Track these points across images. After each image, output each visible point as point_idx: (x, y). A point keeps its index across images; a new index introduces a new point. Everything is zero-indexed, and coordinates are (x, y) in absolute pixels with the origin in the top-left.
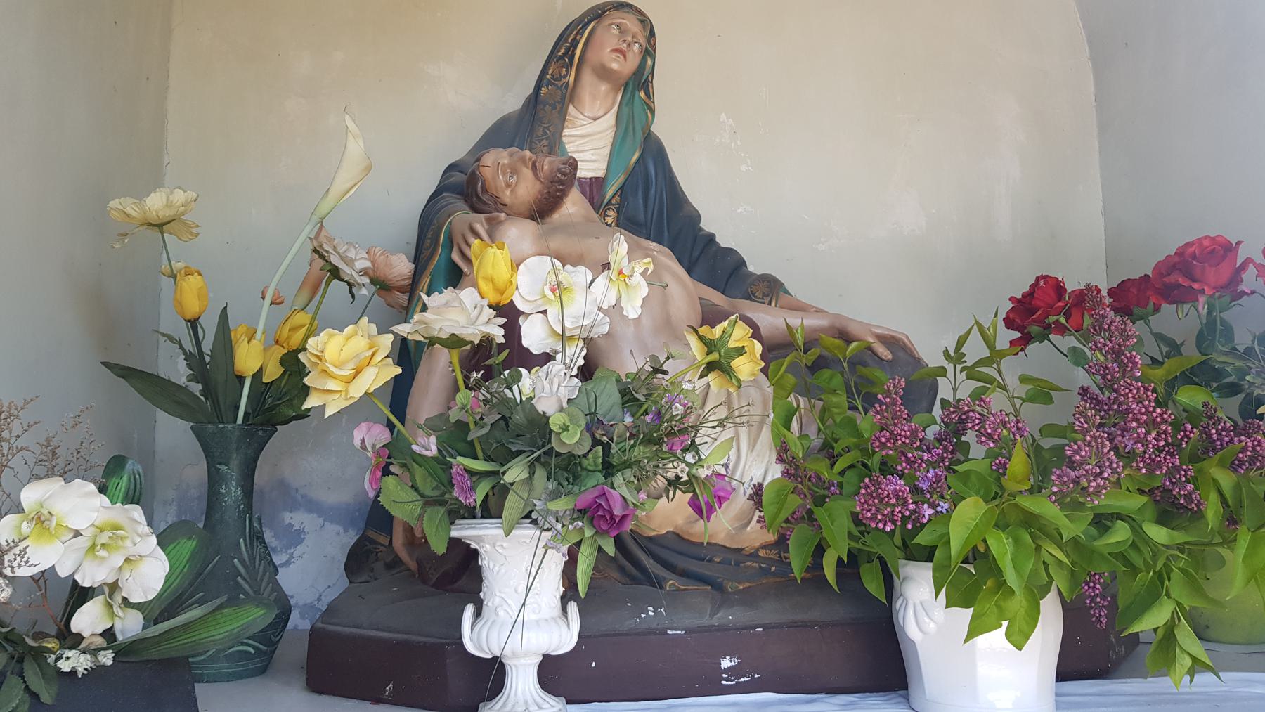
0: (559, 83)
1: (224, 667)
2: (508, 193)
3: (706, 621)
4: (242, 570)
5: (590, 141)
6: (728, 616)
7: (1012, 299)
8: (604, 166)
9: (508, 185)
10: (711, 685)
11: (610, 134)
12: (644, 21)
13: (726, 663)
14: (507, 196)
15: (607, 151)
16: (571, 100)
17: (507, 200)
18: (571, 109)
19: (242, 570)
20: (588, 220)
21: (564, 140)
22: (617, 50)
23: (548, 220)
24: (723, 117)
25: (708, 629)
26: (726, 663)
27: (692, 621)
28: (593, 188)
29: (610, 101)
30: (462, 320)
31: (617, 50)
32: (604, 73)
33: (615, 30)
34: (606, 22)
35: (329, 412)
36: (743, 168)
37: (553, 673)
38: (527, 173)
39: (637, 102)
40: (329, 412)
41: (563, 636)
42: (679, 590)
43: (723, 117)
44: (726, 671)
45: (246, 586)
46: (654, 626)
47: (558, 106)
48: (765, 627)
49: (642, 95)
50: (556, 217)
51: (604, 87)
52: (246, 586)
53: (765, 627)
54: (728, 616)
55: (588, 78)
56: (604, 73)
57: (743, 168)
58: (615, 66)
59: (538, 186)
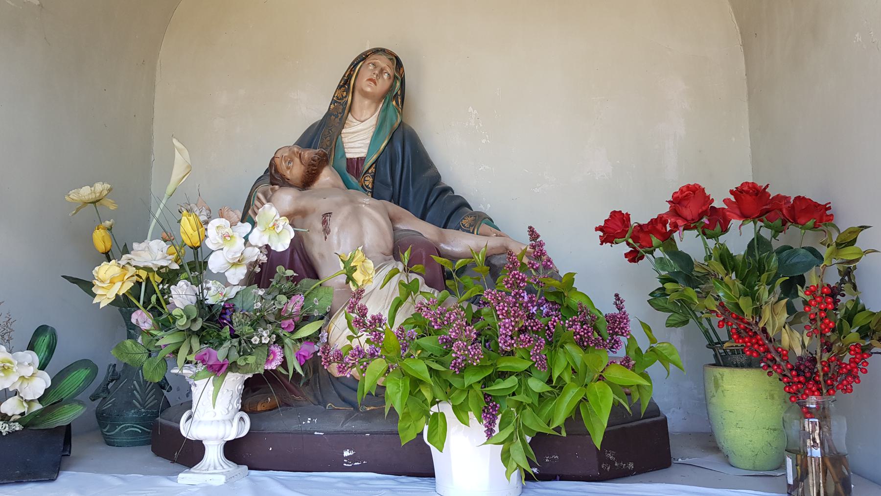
0: (342, 102)
1: (124, 439)
2: (288, 172)
3: (339, 428)
4: (138, 387)
5: (359, 138)
7: (597, 229)
8: (366, 151)
9: (288, 168)
10: (337, 466)
12: (363, 58)
13: (346, 453)
14: (288, 174)
15: (368, 141)
16: (350, 110)
17: (289, 177)
19: (138, 387)
21: (345, 140)
22: (370, 80)
23: (312, 187)
24: (470, 109)
25: (337, 433)
26: (346, 453)
27: (331, 427)
28: (354, 166)
29: (373, 109)
30: (149, 257)
31: (370, 80)
32: (365, 95)
33: (371, 67)
34: (367, 62)
35: (102, 306)
36: (484, 141)
37: (233, 451)
38: (297, 160)
39: (391, 108)
40: (102, 306)
41: (237, 428)
42: (334, 409)
43: (470, 109)
44: (347, 458)
45: (138, 396)
46: (308, 429)
47: (340, 116)
48: (371, 433)
49: (394, 103)
50: (316, 185)
51: (367, 102)
52: (138, 396)
53: (371, 433)
55: (357, 96)
56: (365, 95)
57: (484, 141)
58: (369, 89)
59: (303, 167)
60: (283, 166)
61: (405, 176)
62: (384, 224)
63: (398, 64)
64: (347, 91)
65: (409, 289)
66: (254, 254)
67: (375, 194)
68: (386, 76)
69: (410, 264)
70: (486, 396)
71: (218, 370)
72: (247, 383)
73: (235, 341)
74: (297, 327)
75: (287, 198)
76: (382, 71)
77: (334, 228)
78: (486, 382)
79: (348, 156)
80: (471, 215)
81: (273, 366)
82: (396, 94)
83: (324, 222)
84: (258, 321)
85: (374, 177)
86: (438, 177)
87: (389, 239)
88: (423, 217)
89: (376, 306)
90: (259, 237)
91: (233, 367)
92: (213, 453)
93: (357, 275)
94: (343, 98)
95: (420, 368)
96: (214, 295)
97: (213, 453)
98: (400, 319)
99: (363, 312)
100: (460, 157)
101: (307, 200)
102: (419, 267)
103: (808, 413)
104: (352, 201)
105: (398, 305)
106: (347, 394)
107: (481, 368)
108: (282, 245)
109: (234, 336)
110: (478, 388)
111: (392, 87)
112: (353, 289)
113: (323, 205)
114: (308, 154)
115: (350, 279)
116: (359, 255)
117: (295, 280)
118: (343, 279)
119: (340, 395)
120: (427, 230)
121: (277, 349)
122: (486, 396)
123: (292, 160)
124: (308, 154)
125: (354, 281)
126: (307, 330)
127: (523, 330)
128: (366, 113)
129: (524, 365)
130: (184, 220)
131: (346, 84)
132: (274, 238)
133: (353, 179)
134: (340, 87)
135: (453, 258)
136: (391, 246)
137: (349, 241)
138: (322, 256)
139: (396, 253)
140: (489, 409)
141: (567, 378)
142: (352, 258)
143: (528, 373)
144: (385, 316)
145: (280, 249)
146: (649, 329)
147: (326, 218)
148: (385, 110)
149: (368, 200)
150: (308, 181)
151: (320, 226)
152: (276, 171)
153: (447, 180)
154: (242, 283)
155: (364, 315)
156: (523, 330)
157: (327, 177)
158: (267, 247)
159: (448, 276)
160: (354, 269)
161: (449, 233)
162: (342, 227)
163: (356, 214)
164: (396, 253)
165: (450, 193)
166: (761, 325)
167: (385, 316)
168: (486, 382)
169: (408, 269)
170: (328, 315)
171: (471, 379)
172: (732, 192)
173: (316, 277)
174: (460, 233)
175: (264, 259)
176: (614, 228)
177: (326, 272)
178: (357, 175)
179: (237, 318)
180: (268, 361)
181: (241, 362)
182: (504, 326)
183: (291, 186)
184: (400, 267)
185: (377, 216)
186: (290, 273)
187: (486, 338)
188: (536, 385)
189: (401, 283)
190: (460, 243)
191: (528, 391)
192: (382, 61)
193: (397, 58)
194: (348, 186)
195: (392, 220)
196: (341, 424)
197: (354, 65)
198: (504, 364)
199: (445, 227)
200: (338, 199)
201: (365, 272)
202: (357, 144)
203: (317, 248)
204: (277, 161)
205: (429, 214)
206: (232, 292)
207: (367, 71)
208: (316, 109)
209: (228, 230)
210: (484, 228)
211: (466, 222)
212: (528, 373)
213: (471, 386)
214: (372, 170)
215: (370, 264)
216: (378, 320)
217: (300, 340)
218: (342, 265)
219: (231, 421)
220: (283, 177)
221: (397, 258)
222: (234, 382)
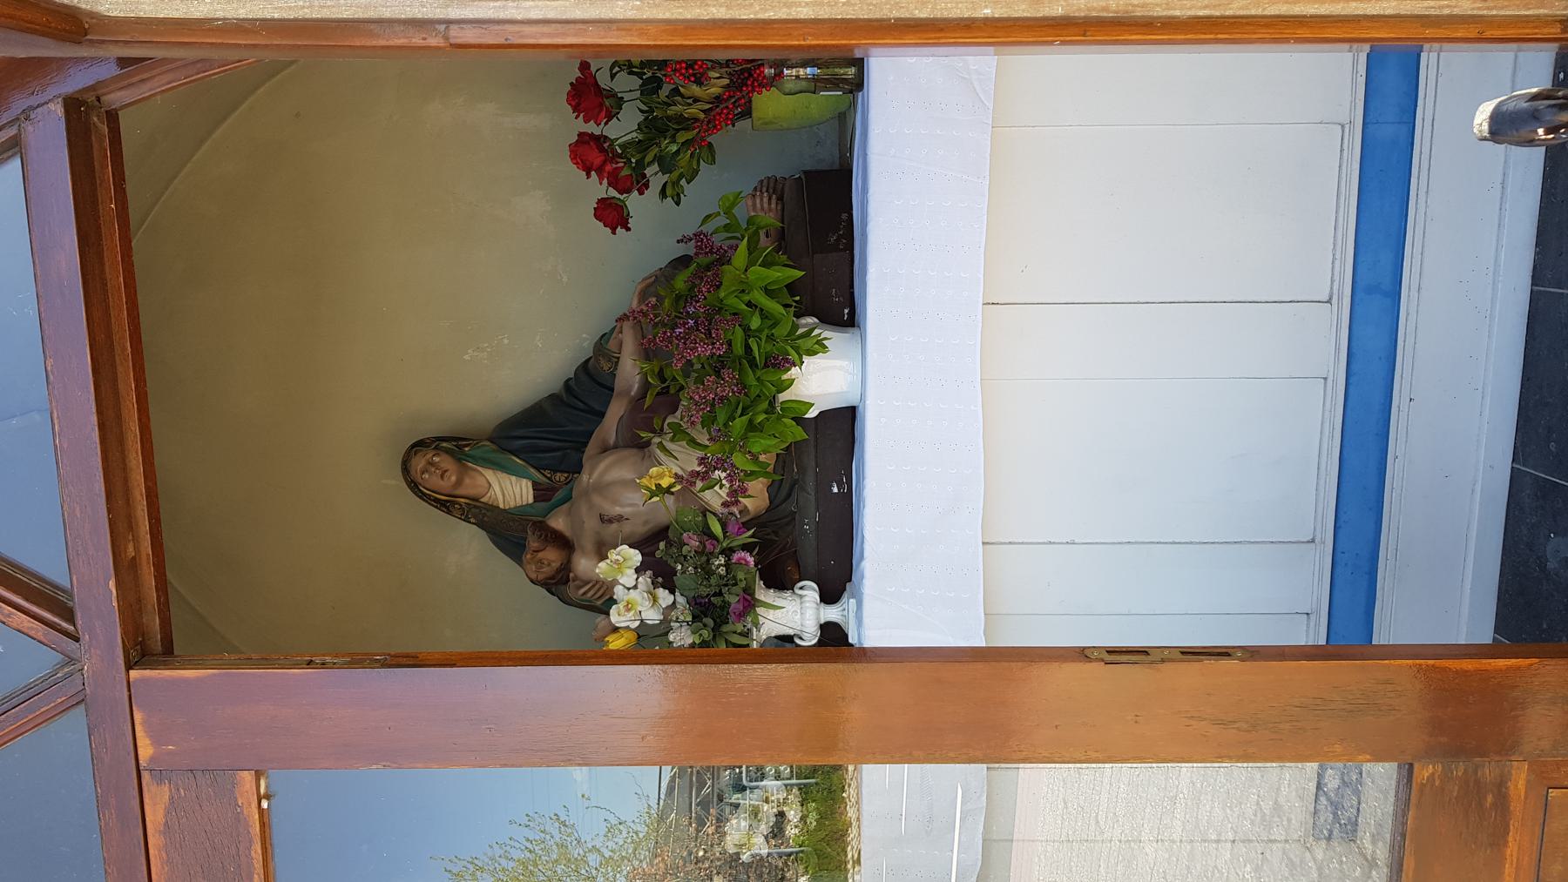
3: (812, 498)
5: (510, 489)
6: (810, 485)
8: (524, 481)
11: (501, 475)
12: (414, 486)
13: (835, 490)
14: (555, 565)
18: (484, 500)
20: (569, 513)
21: (512, 504)
24: (467, 357)
25: (817, 500)
28: (541, 493)
32: (459, 483)
33: (426, 476)
37: (830, 596)
38: (540, 555)
41: (810, 592)
43: (467, 357)
50: (568, 534)
51: (467, 481)
54: (810, 485)
56: (459, 483)
58: (453, 478)
60: (547, 570)
61: (554, 432)
62: (609, 459)
63: (420, 445)
64: (454, 503)
65: (678, 433)
66: (645, 580)
67: (577, 469)
68: (436, 459)
69: (653, 431)
70: (766, 366)
71: (750, 604)
72: (768, 586)
73: (725, 590)
74: (716, 538)
75: (583, 564)
76: (431, 464)
77: (618, 510)
78: (753, 364)
79: (531, 500)
80: (597, 361)
81: (751, 560)
82: (457, 445)
83: (610, 521)
84: (707, 572)
85: (555, 471)
86: (552, 397)
87: (626, 452)
88: (602, 415)
89: (689, 461)
90: (628, 577)
91: (749, 591)
92: (832, 613)
93: (665, 483)
94: (461, 508)
95: (739, 423)
96: (683, 611)
97: (832, 613)
98: (703, 439)
99: (696, 474)
100: (524, 362)
101: (588, 542)
102: (657, 423)
103: (780, 75)
104: (586, 493)
105: (693, 443)
106: (784, 492)
107: (741, 370)
108: (636, 557)
109: (720, 594)
110: (759, 373)
111: (447, 451)
112: (678, 487)
113: (591, 523)
114: (533, 543)
115: (668, 491)
116: (645, 481)
117: (669, 544)
118: (670, 500)
119: (785, 500)
120: (616, 411)
121: (735, 557)
122: (766, 366)
123: (540, 561)
124: (533, 543)
125: (671, 486)
126: (716, 528)
127: (709, 334)
128: (480, 481)
129: (739, 332)
130: (612, 646)
131: (446, 505)
132: (629, 563)
133: (559, 495)
134: (449, 512)
135: (646, 386)
136: (635, 451)
137: (630, 495)
138: (646, 522)
139: (643, 446)
140: (780, 362)
141: (746, 298)
142: (647, 488)
143: (747, 330)
144: (701, 454)
145: (640, 558)
146: (708, 217)
147: (605, 520)
148: (476, 460)
149: (585, 477)
150: (565, 544)
151: (614, 526)
152: (552, 578)
153: (556, 386)
154: (672, 592)
155: (698, 473)
156: (709, 334)
157: (558, 522)
158: (638, 570)
159: (664, 392)
160: (658, 486)
161: (619, 384)
162: (615, 502)
163: (601, 488)
164: (643, 446)
165: (572, 383)
166: (702, 116)
167: (701, 454)
168: (753, 364)
169: (661, 432)
170: (705, 511)
171: (751, 379)
172: (588, 176)
173: (667, 528)
174: (618, 373)
175: (649, 573)
176: (612, 215)
177: (663, 518)
178: (554, 490)
179: (704, 591)
180: (747, 563)
181: (743, 584)
182: (704, 351)
183: (569, 561)
184: (657, 440)
185: (602, 466)
186: (662, 545)
187: (718, 366)
188: (755, 323)
189: (672, 440)
190: (630, 371)
191: (760, 330)
192: (419, 463)
193: (413, 446)
194: (568, 499)
195: (605, 449)
196: (808, 497)
197: (423, 496)
198: (739, 349)
199: (612, 390)
200: (584, 509)
201: (661, 476)
202: (517, 491)
203: (639, 529)
204: (541, 577)
205: (597, 407)
206: (681, 600)
207: (431, 480)
208: (468, 546)
209: (621, 606)
210: (612, 345)
211: (606, 366)
212: (747, 330)
213: (758, 379)
214: (547, 473)
215: (654, 470)
216: (702, 461)
217: (725, 532)
218: (656, 499)
219: (801, 596)
220: (559, 571)
221: (648, 443)
222: (763, 594)
